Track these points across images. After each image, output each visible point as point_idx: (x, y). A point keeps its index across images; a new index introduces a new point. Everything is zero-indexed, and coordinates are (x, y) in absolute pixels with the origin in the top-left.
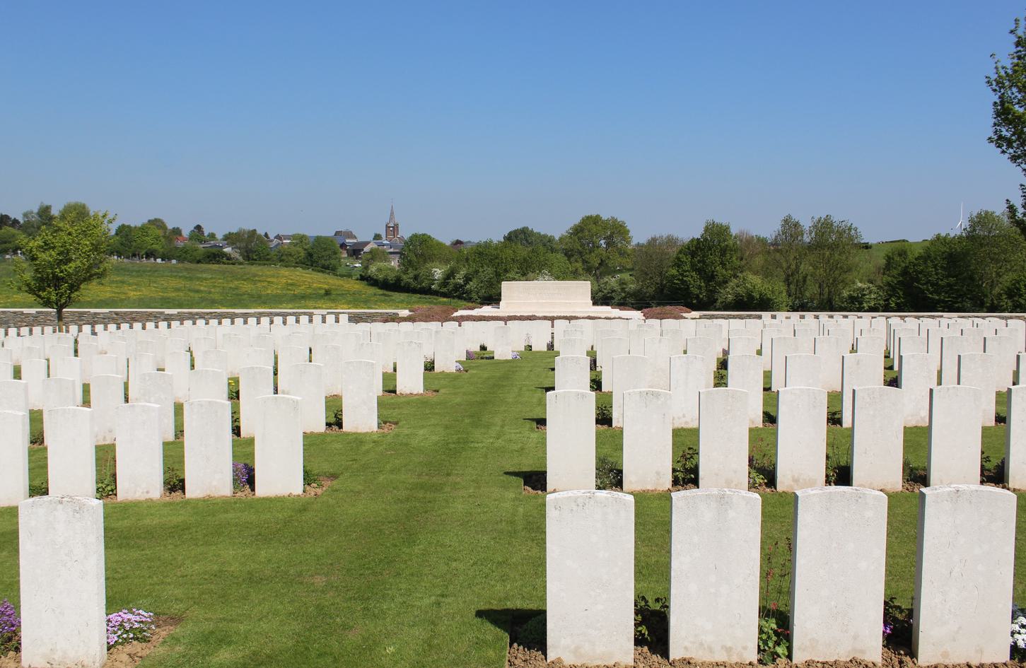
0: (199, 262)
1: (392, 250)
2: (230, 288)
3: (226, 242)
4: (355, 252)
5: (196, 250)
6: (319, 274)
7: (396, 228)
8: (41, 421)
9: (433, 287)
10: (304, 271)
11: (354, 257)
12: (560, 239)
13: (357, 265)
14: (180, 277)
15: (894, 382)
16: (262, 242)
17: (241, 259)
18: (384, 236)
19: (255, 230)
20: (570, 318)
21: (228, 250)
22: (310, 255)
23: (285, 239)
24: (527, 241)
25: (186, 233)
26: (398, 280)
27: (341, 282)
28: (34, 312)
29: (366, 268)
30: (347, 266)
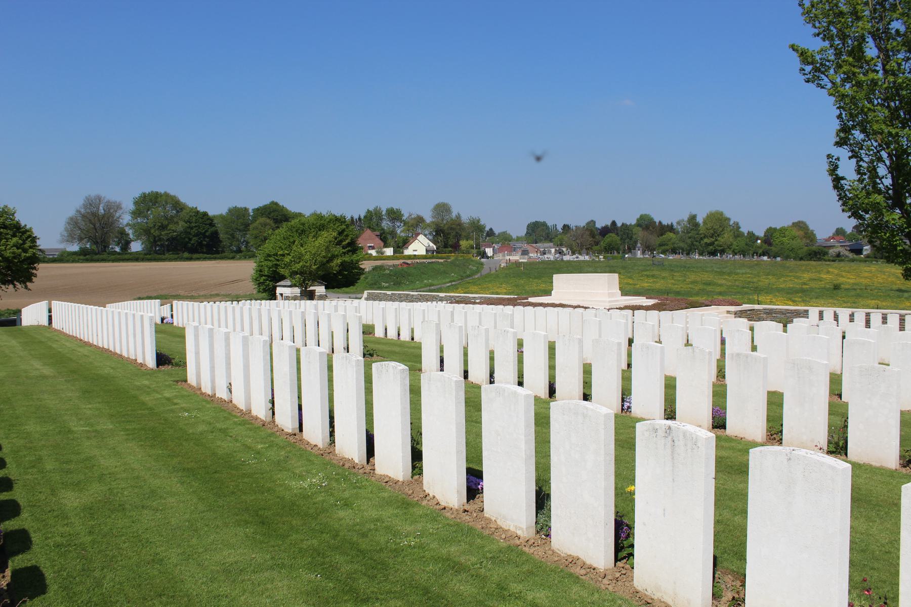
0: (801, 259)
8: (781, 405)
12: (499, 234)
15: (586, 397)
19: (368, 210)
20: (586, 308)
28: (390, 294)
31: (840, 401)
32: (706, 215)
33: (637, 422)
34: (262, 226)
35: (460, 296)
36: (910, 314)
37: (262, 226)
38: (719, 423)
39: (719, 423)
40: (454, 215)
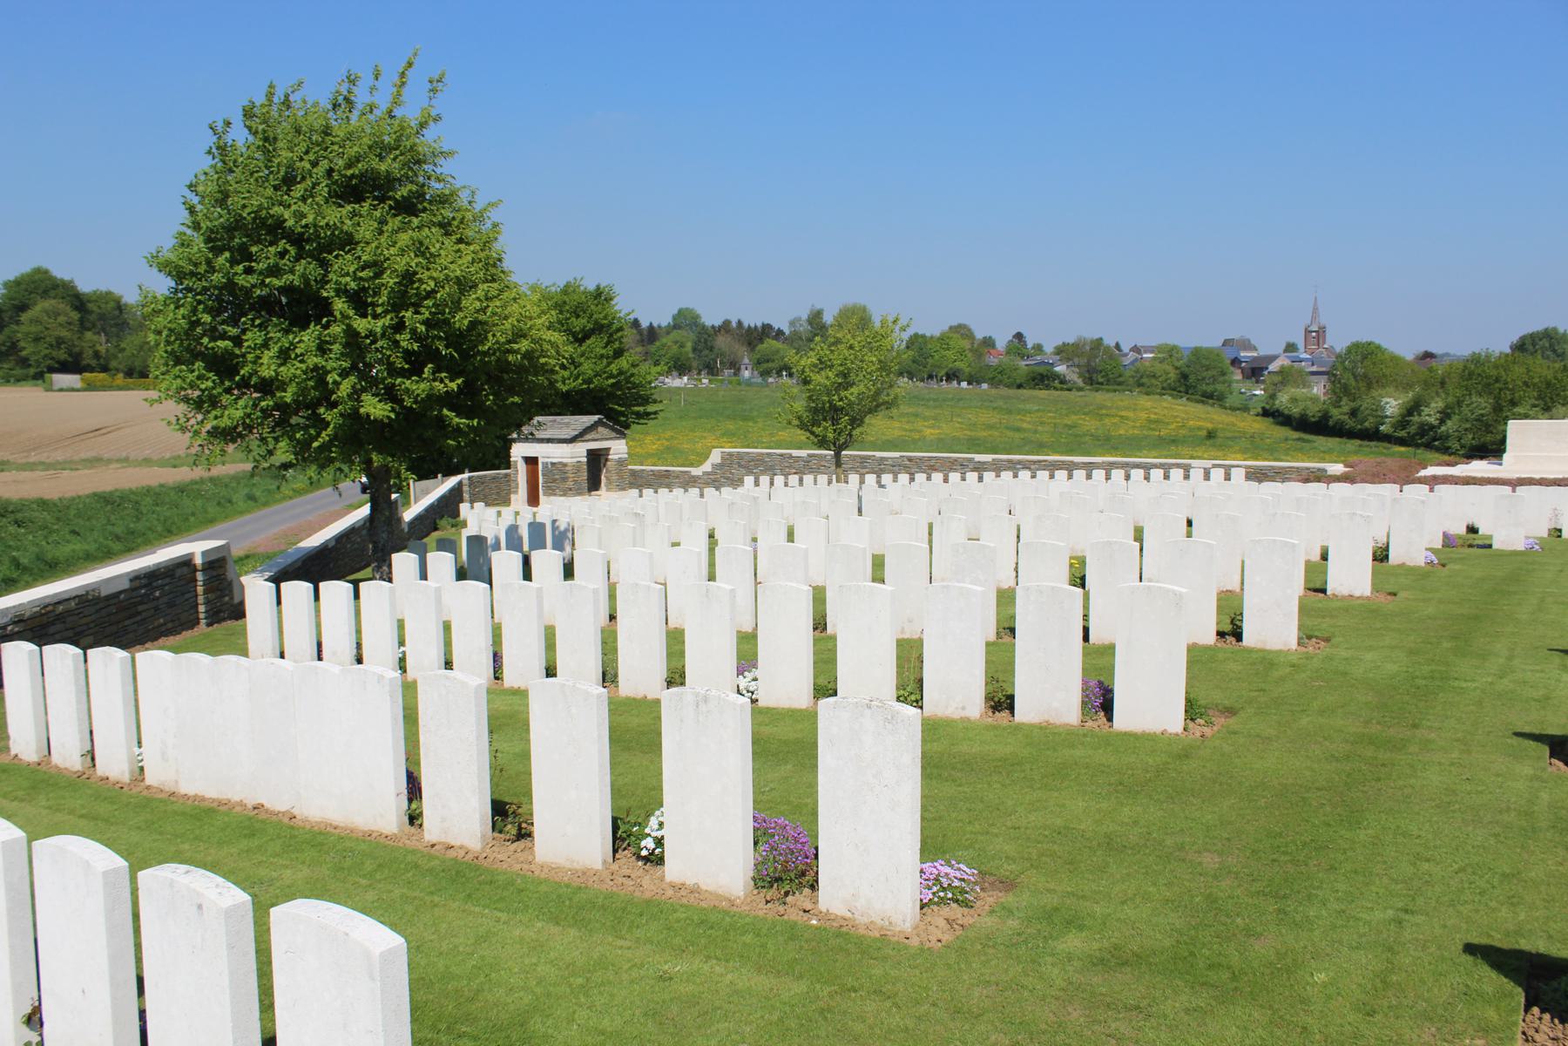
0: (1020, 386)
1: (1314, 369)
2: (1066, 425)
3: (1058, 357)
4: (1255, 372)
5: (1016, 369)
6: (1197, 405)
7: (1321, 334)
9: (1382, 428)
10: (1173, 401)
11: (1254, 379)
13: (1257, 392)
14: (994, 409)
16: (1111, 357)
17: (1080, 382)
18: (1301, 346)
19: (1101, 339)
21: (1061, 369)
22: (1185, 376)
23: (1146, 352)
24: (1554, 351)
25: (1001, 344)
26: (1326, 416)
27: (1232, 419)
29: (1273, 397)
30: (1241, 393)
31: (1106, 728)
33: (273, 905)
35: (1045, 461)
37: (50, 318)
40: (163, 285)
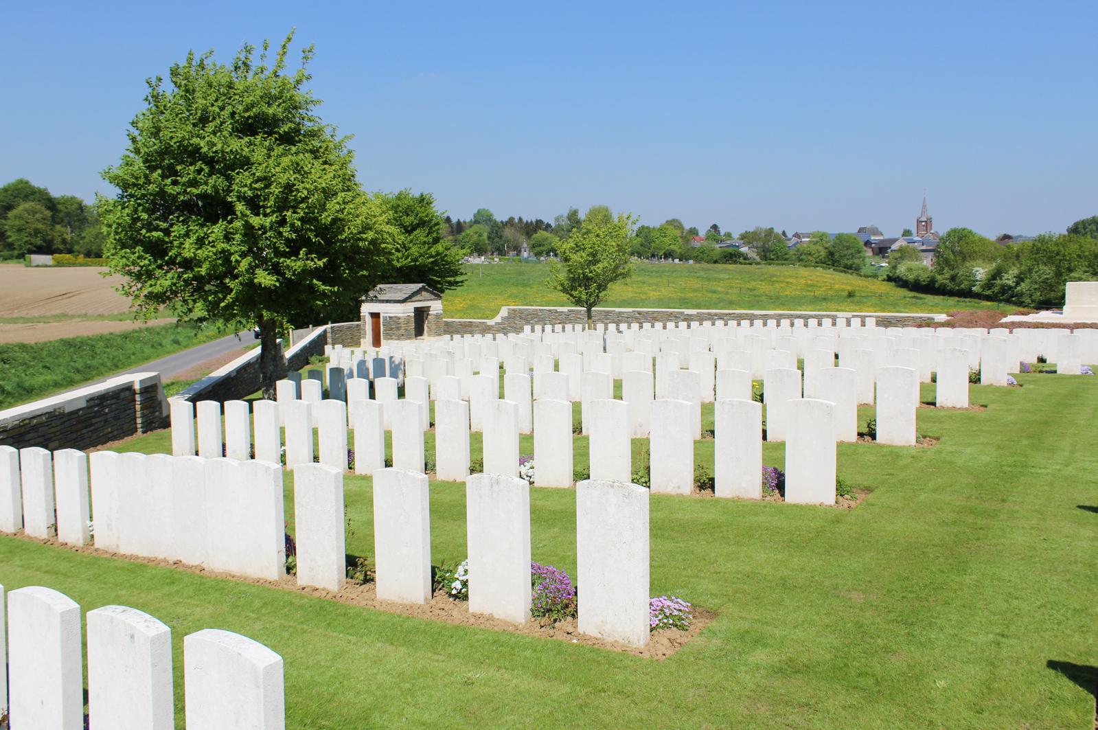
0: (716, 262)
28: (695, 313)
32: (588, 210)
34: (29, 215)
35: (734, 314)
36: (1092, 326)
38: (429, 467)
39: (429, 467)
